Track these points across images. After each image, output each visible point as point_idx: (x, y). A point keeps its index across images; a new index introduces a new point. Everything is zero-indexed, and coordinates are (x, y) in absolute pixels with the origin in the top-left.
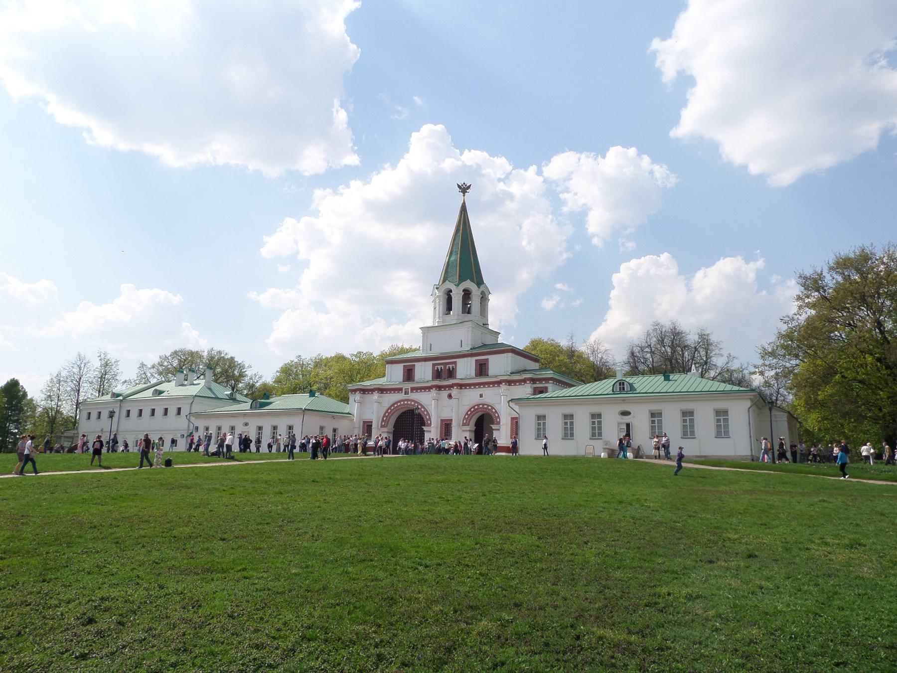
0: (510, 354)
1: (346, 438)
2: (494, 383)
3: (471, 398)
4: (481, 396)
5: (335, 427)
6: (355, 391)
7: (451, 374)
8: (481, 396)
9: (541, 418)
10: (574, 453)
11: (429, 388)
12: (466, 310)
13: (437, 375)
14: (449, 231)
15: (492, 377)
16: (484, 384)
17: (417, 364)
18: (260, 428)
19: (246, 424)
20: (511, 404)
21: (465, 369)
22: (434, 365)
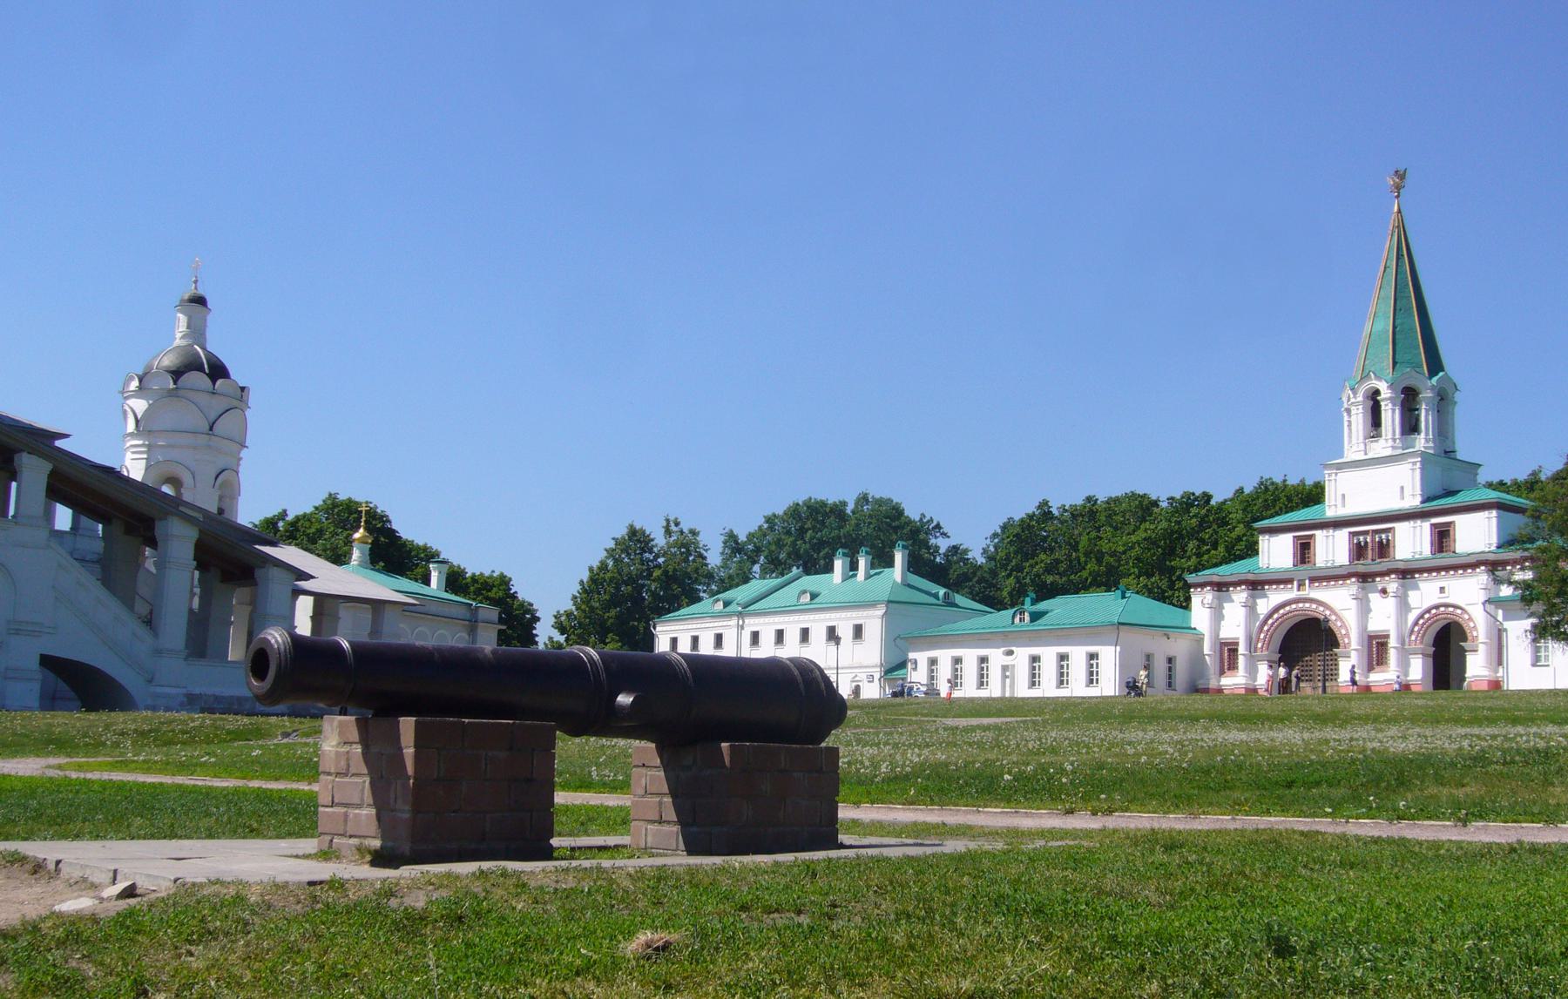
0: (1494, 513)
1: (985, 551)
2: (1464, 567)
3: (1426, 594)
4: (1442, 589)
5: (1171, 654)
6: (1202, 585)
7: (1384, 549)
8: (1442, 589)
9: (1063, 657)
10: (1551, 687)
11: (1349, 576)
12: (1410, 426)
13: (1359, 551)
14: (1389, 245)
15: (1461, 556)
16: (1447, 568)
17: (1319, 534)
18: (983, 660)
19: (1010, 653)
20: (1490, 608)
21: (1411, 542)
22: (1353, 534)
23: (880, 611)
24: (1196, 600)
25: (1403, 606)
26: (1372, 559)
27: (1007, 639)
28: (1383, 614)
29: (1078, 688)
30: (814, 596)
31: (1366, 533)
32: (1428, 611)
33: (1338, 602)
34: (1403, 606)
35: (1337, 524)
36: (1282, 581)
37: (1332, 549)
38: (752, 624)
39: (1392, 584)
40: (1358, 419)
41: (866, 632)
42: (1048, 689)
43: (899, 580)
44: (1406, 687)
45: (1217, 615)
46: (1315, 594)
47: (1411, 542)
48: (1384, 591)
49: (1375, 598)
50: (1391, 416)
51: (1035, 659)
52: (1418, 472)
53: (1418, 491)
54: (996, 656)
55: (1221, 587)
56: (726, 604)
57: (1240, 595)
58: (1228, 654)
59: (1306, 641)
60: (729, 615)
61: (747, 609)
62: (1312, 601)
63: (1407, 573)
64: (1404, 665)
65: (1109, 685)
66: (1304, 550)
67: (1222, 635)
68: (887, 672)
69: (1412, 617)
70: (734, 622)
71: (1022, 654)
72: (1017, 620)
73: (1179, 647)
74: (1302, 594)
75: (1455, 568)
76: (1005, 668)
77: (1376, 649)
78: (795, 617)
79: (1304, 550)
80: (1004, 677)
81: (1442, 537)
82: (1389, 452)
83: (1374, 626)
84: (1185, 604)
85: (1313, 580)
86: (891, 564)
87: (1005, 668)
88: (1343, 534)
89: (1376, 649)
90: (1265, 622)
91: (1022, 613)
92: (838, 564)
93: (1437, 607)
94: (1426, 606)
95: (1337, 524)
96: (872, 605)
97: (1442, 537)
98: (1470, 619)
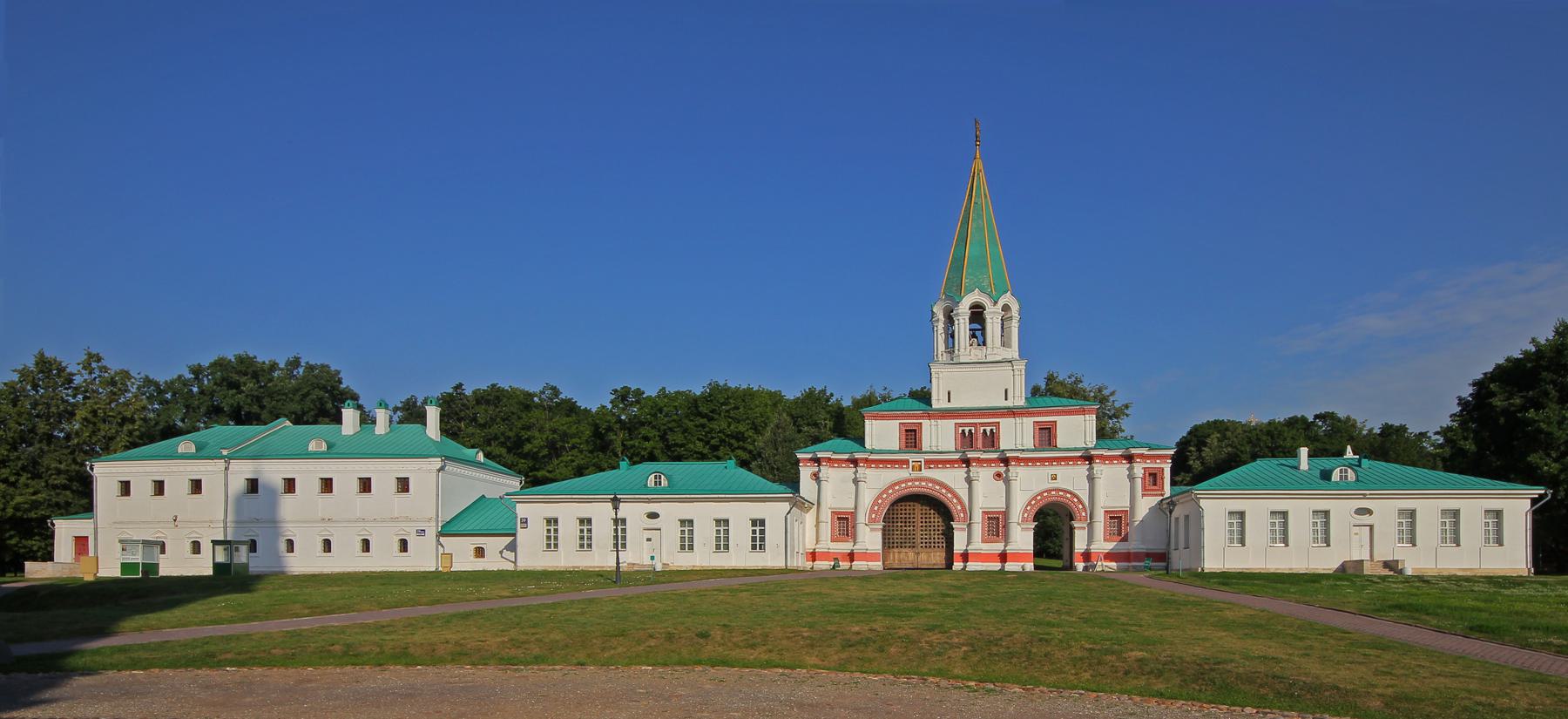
4: (1054, 478)
7: (992, 440)
13: (967, 440)
26: (978, 441)
37: (939, 436)
47: (1017, 435)
66: (912, 438)
79: (912, 438)
81: (1047, 434)
88: (949, 425)
97: (1047, 434)
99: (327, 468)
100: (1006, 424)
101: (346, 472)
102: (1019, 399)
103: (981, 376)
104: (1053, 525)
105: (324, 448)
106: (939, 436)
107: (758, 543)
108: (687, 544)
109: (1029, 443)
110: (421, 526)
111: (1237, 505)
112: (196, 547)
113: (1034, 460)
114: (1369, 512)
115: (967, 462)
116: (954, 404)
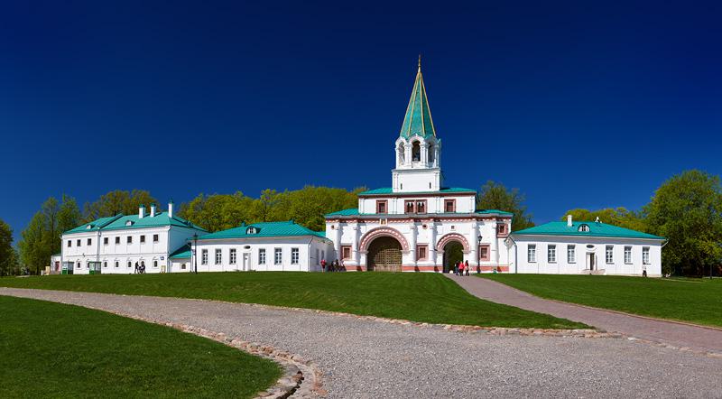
3: (445, 228)
4: (453, 227)
7: (421, 208)
13: (409, 208)
16: (451, 218)
17: (389, 200)
19: (248, 247)
23: (168, 228)
24: (328, 226)
25: (435, 233)
26: (415, 211)
27: (246, 239)
28: (426, 235)
29: (287, 266)
30: (133, 223)
31: (413, 201)
32: (446, 236)
33: (404, 231)
34: (435, 233)
35: (399, 196)
36: (372, 219)
37: (396, 207)
38: (105, 235)
39: (430, 224)
40: (408, 152)
41: (160, 238)
42: (270, 266)
43: (171, 216)
44: (359, 268)
45: (341, 232)
46: (390, 226)
47: (435, 206)
48: (425, 226)
49: (420, 227)
50: (424, 152)
51: (262, 251)
52: (438, 178)
53: (438, 185)
54: (240, 249)
55: (343, 221)
56: (92, 227)
57: (352, 226)
58: (346, 250)
59: (383, 246)
60: (94, 231)
61: (102, 228)
62: (389, 228)
63: (437, 219)
64: (358, 258)
65: (304, 265)
66: (381, 207)
67: (419, 241)
68: (170, 256)
69: (438, 238)
70: (96, 233)
71: (255, 248)
72: (249, 232)
73: (324, 247)
74: (383, 225)
75: (455, 218)
76: (245, 255)
77: (421, 251)
78: (125, 232)
79: (381, 207)
80: (245, 259)
81: (449, 205)
82: (424, 167)
83: (420, 241)
84: (323, 229)
85: (389, 220)
86: (167, 210)
87: (245, 255)
88: (402, 200)
89: (421, 251)
90: (364, 237)
91: (251, 228)
92: (141, 210)
93: (450, 234)
94: (457, 232)
95: (399, 196)
96: (163, 226)
97: (449, 205)
98: (466, 240)
99: (117, 234)
100: (430, 200)
101: (136, 235)
102: (436, 188)
103: (415, 175)
104: (453, 251)
105: (129, 224)
106: (396, 207)
107: (232, 260)
108: (262, 261)
109: (442, 210)
110: (162, 255)
111: (295, 246)
112: (130, 264)
113: (405, 219)
114: (249, 247)
115: (478, 219)
116: (405, 191)
